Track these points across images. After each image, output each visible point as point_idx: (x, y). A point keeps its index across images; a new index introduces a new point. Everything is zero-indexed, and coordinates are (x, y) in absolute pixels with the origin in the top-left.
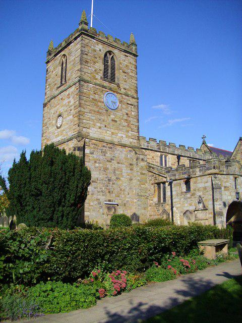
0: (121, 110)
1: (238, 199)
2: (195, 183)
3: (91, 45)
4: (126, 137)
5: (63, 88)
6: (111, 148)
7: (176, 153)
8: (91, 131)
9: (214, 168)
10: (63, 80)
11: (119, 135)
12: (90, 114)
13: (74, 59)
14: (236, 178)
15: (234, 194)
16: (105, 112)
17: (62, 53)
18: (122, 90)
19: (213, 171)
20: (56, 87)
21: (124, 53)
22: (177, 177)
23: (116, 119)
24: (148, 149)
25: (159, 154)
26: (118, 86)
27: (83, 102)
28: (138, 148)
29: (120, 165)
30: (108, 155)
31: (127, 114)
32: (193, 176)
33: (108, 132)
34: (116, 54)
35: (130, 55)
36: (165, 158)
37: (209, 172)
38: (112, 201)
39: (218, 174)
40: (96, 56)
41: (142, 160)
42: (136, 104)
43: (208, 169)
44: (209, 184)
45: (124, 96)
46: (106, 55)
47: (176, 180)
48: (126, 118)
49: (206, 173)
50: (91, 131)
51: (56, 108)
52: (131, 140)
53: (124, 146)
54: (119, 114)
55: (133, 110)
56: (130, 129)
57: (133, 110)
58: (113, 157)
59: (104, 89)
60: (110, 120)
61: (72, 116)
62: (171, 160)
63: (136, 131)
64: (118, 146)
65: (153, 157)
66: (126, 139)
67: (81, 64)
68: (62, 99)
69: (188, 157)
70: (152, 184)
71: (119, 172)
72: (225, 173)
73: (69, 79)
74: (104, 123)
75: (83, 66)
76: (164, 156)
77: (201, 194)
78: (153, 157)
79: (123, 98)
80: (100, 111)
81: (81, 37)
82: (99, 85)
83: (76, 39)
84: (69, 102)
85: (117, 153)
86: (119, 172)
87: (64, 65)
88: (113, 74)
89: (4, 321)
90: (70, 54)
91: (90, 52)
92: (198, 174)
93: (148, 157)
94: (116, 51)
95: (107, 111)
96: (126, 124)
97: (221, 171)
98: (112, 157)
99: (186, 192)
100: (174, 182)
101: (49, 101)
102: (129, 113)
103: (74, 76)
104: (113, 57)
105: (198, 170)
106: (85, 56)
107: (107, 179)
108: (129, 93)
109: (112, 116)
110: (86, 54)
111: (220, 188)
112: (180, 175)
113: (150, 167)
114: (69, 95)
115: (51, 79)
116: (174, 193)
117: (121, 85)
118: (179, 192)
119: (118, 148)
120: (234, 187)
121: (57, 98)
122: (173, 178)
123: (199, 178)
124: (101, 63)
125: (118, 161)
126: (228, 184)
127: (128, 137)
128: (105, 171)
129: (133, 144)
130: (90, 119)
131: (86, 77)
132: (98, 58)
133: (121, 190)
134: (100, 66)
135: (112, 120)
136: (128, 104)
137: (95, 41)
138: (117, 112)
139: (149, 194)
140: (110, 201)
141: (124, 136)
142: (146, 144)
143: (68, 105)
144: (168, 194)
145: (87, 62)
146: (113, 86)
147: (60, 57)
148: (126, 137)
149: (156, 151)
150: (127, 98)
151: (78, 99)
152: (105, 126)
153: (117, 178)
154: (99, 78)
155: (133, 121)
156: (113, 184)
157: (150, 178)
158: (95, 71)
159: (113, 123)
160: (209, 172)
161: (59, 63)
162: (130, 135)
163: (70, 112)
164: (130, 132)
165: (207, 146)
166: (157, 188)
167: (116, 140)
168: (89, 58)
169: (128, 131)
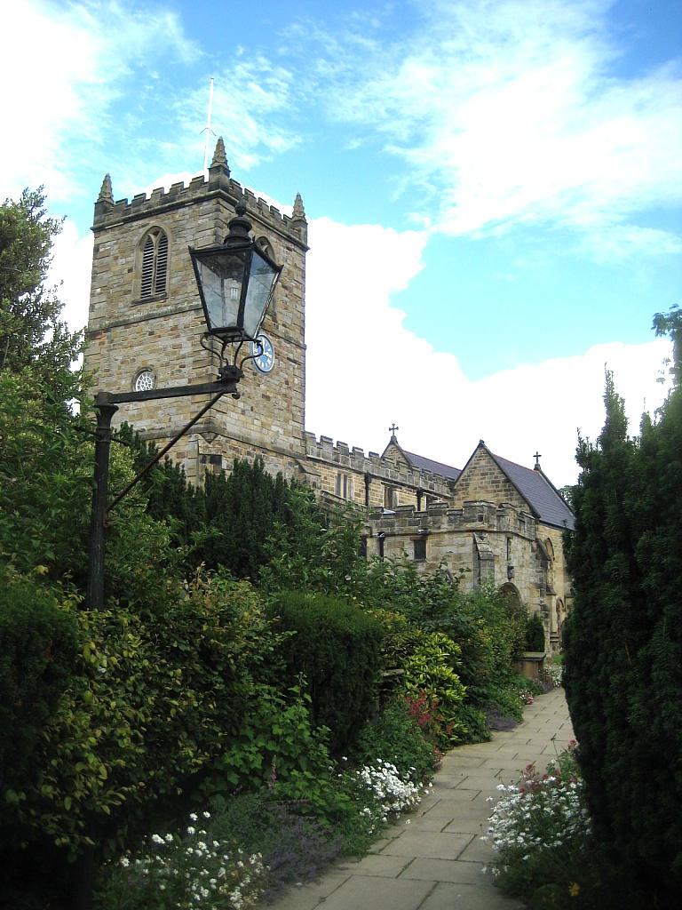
0: (277, 374)
1: (509, 579)
2: (438, 544)
5: (147, 309)
8: (228, 419)
9: (481, 519)
11: (274, 428)
14: (508, 539)
16: (252, 376)
18: (281, 327)
19: (478, 525)
20: (129, 298)
21: (286, 243)
22: (396, 529)
23: (268, 394)
25: (335, 471)
28: (303, 458)
31: (287, 383)
32: (433, 531)
34: (273, 244)
35: (296, 249)
37: (469, 526)
43: (467, 520)
44: (468, 549)
47: (393, 535)
48: (284, 391)
49: (462, 528)
50: (228, 419)
51: (131, 352)
54: (275, 381)
68: (151, 333)
69: (384, 479)
74: (249, 401)
78: (325, 478)
79: (280, 346)
83: (198, 201)
89: (369, 856)
92: (445, 527)
95: (255, 374)
96: (285, 404)
97: (490, 526)
101: (107, 330)
102: (290, 380)
105: (445, 519)
108: (291, 334)
112: (403, 524)
114: (175, 328)
117: (279, 317)
122: (387, 530)
123: (446, 536)
127: (286, 433)
129: (295, 449)
135: (263, 396)
138: (271, 377)
143: (174, 353)
149: (332, 465)
150: (288, 345)
159: (265, 402)
160: (469, 526)
161: (141, 242)
165: (399, 449)
169: (287, 421)
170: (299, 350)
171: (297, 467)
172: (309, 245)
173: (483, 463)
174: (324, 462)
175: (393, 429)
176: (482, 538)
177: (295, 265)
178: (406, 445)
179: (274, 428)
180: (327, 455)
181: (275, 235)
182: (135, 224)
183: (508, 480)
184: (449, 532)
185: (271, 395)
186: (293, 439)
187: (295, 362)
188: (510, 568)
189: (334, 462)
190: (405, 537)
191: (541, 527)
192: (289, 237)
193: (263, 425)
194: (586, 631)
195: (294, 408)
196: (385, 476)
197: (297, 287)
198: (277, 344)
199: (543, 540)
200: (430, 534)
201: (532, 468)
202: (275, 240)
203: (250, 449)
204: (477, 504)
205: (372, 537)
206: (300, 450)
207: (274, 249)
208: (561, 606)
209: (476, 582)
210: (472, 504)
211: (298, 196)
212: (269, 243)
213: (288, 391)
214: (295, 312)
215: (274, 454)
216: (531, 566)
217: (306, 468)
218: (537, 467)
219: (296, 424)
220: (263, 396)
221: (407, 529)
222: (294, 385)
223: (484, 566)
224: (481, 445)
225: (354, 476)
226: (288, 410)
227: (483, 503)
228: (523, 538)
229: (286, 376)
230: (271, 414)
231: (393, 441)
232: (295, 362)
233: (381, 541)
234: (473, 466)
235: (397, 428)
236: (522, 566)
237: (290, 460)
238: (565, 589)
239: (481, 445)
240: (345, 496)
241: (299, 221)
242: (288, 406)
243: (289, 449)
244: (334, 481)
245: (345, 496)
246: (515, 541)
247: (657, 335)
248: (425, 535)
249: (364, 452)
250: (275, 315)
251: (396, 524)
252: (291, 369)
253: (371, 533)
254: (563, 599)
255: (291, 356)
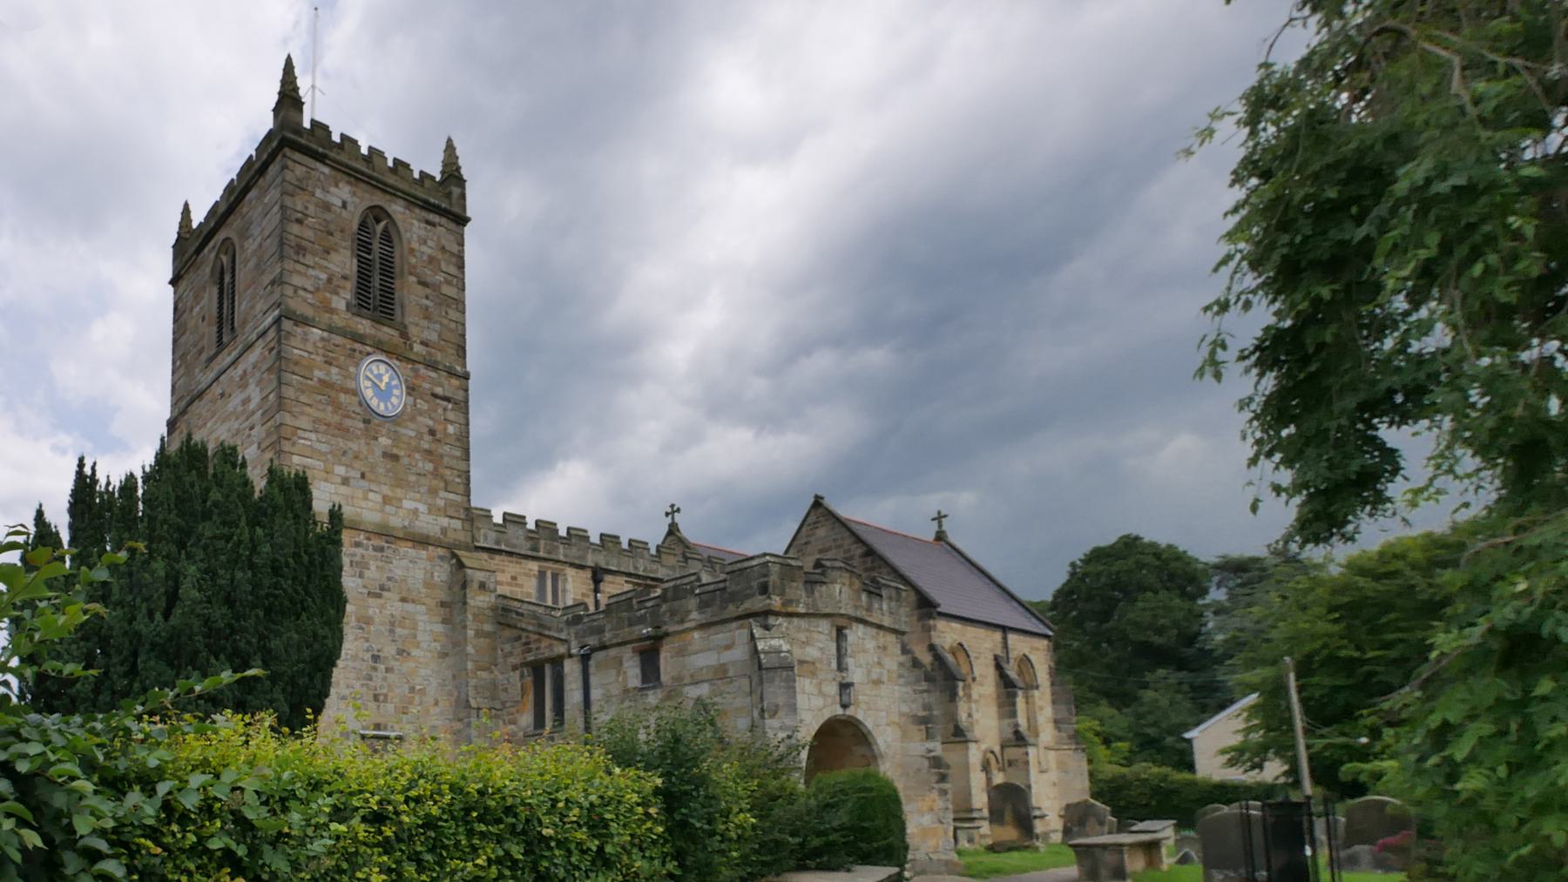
1: (845, 706)
2: (682, 652)
3: (315, 186)
4: (430, 512)
5: (225, 359)
6: (381, 549)
7: (590, 563)
10: (226, 330)
11: (408, 504)
12: (313, 436)
13: (260, 246)
15: (833, 689)
16: (361, 425)
17: (221, 236)
18: (417, 348)
19: (758, 603)
20: (204, 356)
21: (424, 214)
23: (395, 451)
24: (499, 552)
25: (534, 566)
26: (404, 335)
27: (289, 392)
28: (467, 548)
29: (409, 607)
30: (372, 573)
31: (432, 432)
33: (371, 495)
34: (398, 218)
35: (444, 221)
36: (555, 577)
38: (385, 729)
39: (777, 614)
40: (332, 227)
41: (482, 586)
42: (460, 395)
43: (734, 598)
44: (740, 653)
45: (423, 370)
46: (363, 225)
47: (603, 647)
48: (426, 446)
49: (726, 615)
52: (445, 521)
53: (422, 541)
55: (451, 416)
56: (442, 485)
57: (451, 416)
58: (389, 579)
59: (357, 346)
60: (378, 453)
61: (256, 445)
62: (575, 587)
63: (461, 489)
64: (402, 544)
65: (514, 578)
66: (430, 518)
67: (282, 258)
68: (222, 395)
69: (629, 575)
70: (515, 668)
71: (406, 632)
72: (801, 609)
73: (244, 323)
74: (357, 464)
75: (289, 265)
76: (549, 575)
77: (704, 690)
80: (348, 422)
81: (279, 157)
82: (343, 332)
84: (246, 401)
85: (398, 568)
86: (406, 632)
87: (227, 279)
88: (388, 294)
90: (244, 234)
91: (312, 209)
93: (500, 577)
94: (397, 209)
95: (367, 422)
96: (429, 467)
98: (384, 580)
99: (641, 689)
100: (599, 656)
102: (439, 428)
103: (260, 306)
104: (385, 230)
106: (295, 229)
107: (368, 656)
108: (439, 356)
109: (384, 441)
110: (299, 221)
111: (792, 668)
113: (506, 610)
115: (188, 334)
116: (595, 694)
117: (413, 331)
118: (615, 690)
119: (403, 550)
120: (834, 665)
121: (207, 397)
122: (592, 641)
123: (696, 635)
124: (348, 253)
125: (404, 594)
126: (812, 653)
128: (361, 628)
130: (313, 453)
131: (299, 306)
132: (338, 235)
133: (412, 690)
134: (344, 262)
136: (435, 396)
137: (326, 170)
139: (503, 703)
140: (377, 727)
141: (422, 508)
142: (492, 535)
143: (243, 412)
144: (573, 696)
145: (300, 249)
146: (387, 333)
147: (213, 255)
148: (430, 512)
150: (433, 374)
151: (275, 384)
152: (363, 476)
153: (401, 652)
154: (342, 305)
155: (449, 451)
156: (387, 670)
157: (508, 647)
158: (329, 280)
162: (441, 503)
163: (249, 436)
164: (442, 494)
166: (529, 680)
167: (397, 521)
168: (309, 234)
169: (433, 492)
170: (455, 382)
171: (454, 561)
172: (469, 214)
173: (821, 532)
174: (510, 554)
175: (673, 512)
176: (767, 628)
177: (443, 248)
178: (688, 531)
179: (408, 504)
180: (515, 541)
181: (401, 202)
182: (206, 250)
183: (870, 552)
184: (702, 626)
185: (402, 453)
186: (447, 519)
187: (448, 399)
188: (845, 687)
189: (530, 553)
190: (623, 648)
191: (941, 624)
192: (426, 202)
193: (386, 500)
194: (359, 702)
195: (448, 472)
196: (632, 570)
197: (449, 283)
198: (412, 374)
199: (947, 646)
200: (667, 634)
201: (931, 537)
202: (401, 209)
203: (362, 537)
204: (754, 563)
205: (570, 656)
206: (463, 537)
207: (400, 224)
208: (993, 761)
209: (756, 713)
210: (746, 564)
211: (449, 141)
212: (389, 216)
213: (433, 447)
214: (445, 322)
215: (410, 544)
216: (902, 681)
217: (467, 562)
218: (940, 536)
219: (452, 496)
220: (385, 455)
221: (627, 633)
222: (446, 435)
223: (772, 681)
224: (818, 503)
225: (570, 572)
226: (436, 474)
227: (768, 558)
228: (880, 627)
229: (431, 423)
230: (400, 483)
231: (673, 530)
232: (448, 399)
233: (585, 659)
234: (804, 541)
235: (678, 510)
236: (878, 682)
237: (441, 551)
238: (1001, 731)
239: (818, 503)
240: (555, 599)
241: (453, 176)
242: (436, 469)
243: (439, 535)
244: (534, 582)
245: (555, 599)
246: (856, 634)
247: (1231, 186)
248: (657, 639)
249: (589, 534)
250: (405, 327)
251: (608, 627)
252: (440, 411)
253: (569, 649)
254: (997, 749)
255: (439, 390)
